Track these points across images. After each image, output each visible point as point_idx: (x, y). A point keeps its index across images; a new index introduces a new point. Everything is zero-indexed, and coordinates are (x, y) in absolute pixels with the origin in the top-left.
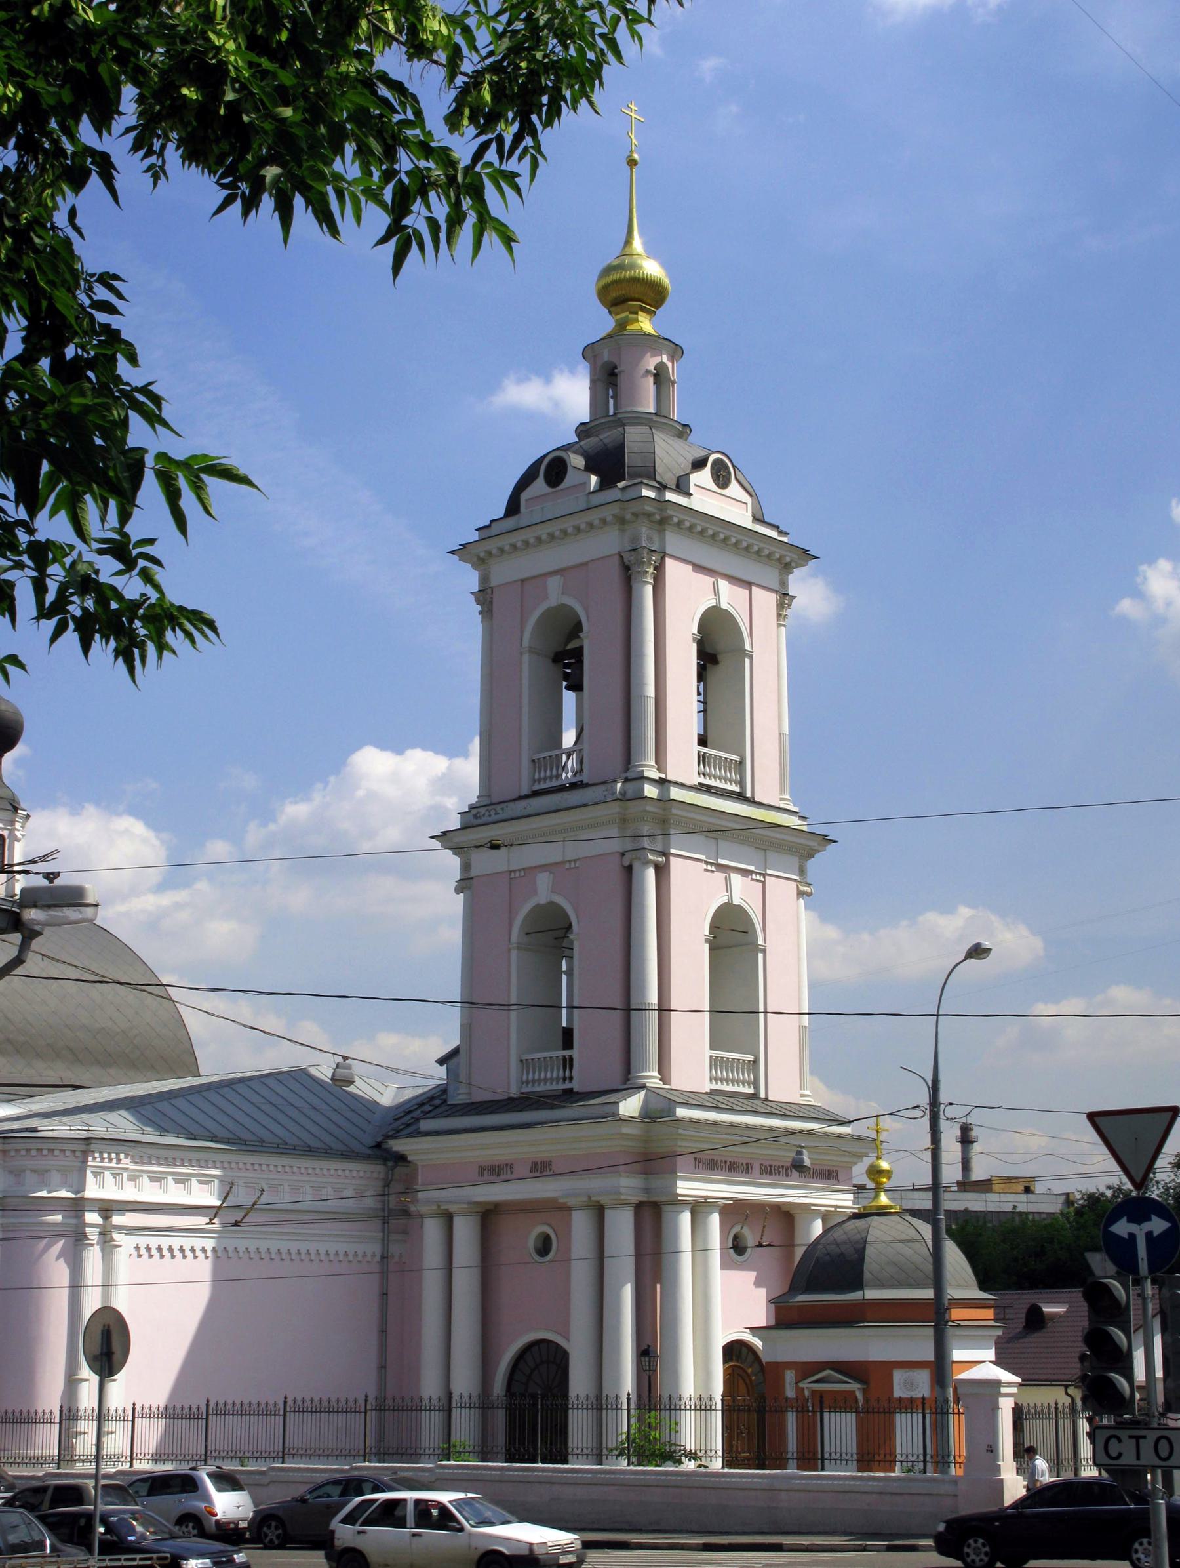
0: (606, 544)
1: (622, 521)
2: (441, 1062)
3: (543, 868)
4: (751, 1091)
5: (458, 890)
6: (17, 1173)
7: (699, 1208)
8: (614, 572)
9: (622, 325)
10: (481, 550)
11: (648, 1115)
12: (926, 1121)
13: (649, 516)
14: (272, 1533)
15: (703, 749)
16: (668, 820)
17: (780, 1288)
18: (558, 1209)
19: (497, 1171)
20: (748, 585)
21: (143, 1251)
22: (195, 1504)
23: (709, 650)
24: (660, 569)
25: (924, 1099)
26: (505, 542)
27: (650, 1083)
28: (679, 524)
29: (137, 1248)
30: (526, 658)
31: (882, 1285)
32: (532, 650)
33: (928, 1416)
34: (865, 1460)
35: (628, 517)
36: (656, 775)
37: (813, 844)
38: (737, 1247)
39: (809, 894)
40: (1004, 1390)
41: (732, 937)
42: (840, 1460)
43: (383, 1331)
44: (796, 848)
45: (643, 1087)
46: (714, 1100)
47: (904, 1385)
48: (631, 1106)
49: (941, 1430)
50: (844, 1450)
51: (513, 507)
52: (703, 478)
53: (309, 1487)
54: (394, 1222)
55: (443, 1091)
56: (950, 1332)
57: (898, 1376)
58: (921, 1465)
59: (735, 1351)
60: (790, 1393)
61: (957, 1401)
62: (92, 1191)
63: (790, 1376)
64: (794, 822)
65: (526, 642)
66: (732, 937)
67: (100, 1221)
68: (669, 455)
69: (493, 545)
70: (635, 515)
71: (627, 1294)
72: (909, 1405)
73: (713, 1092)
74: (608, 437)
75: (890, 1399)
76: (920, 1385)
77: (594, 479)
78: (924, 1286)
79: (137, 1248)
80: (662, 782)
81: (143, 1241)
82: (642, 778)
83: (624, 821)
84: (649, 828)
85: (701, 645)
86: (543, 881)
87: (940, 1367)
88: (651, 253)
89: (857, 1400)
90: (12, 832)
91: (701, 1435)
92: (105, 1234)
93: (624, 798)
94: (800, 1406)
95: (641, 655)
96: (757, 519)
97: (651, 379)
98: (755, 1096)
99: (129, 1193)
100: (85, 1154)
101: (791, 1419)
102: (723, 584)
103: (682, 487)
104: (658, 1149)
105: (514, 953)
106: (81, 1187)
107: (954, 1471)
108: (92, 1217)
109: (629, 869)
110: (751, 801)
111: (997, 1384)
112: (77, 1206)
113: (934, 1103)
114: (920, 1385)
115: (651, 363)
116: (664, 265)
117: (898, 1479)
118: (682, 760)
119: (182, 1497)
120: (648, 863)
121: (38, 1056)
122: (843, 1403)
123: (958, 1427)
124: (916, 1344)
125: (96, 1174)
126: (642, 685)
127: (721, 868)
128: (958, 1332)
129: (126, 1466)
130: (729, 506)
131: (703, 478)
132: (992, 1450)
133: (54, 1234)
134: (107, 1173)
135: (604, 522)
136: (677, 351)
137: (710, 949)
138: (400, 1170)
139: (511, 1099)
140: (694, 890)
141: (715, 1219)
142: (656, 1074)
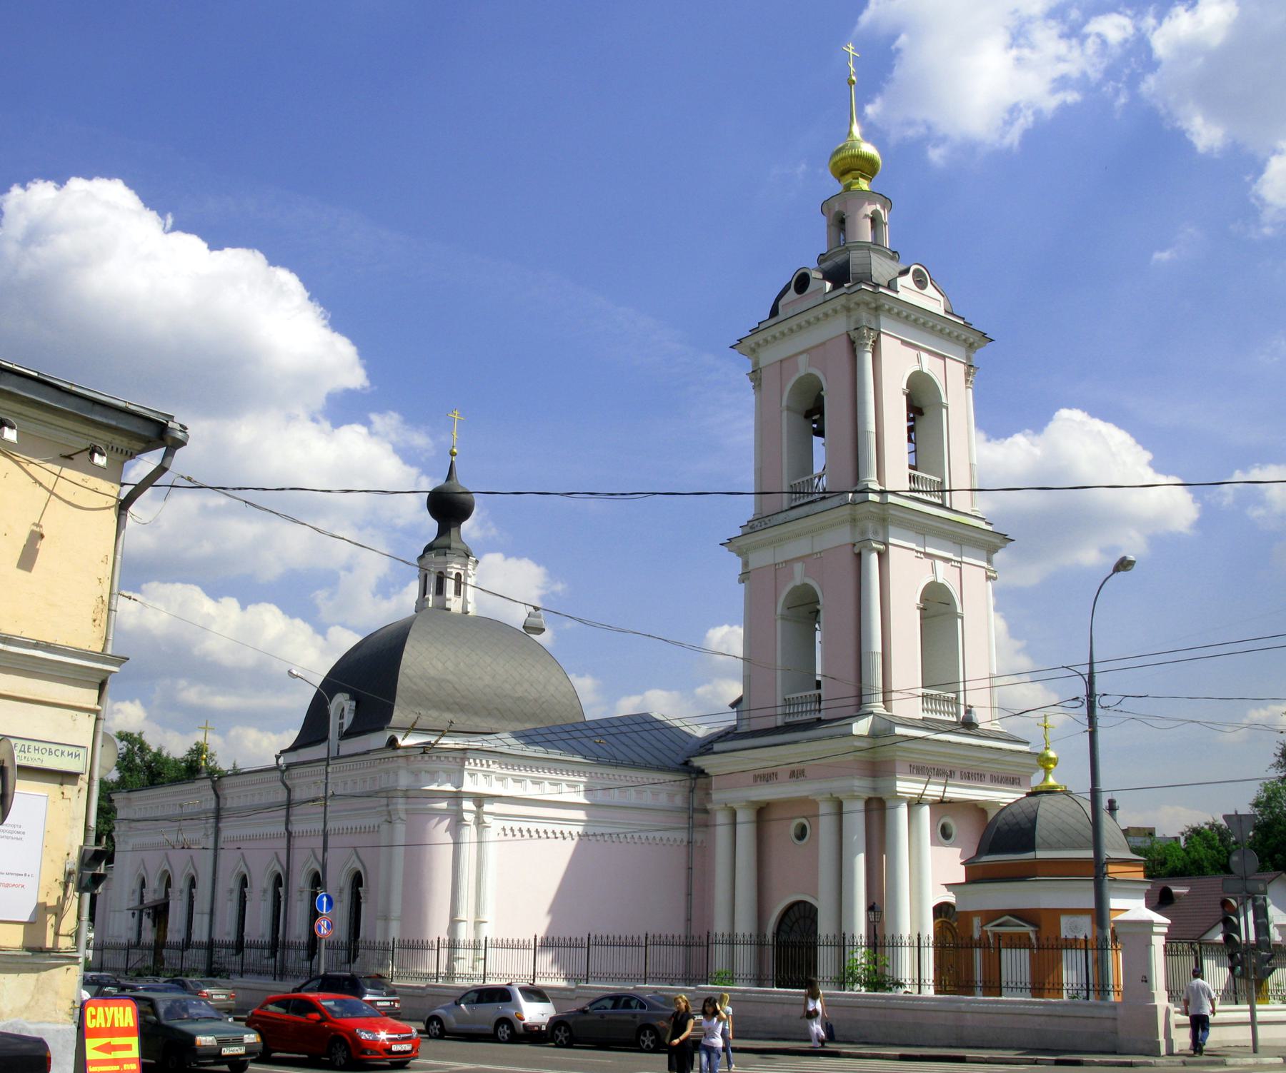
0: (838, 327)
1: (848, 309)
2: (733, 705)
5: (742, 581)
6: (416, 774)
7: (915, 803)
8: (844, 345)
9: (848, 188)
10: (751, 342)
11: (874, 734)
12: (1084, 710)
13: (867, 304)
14: (562, 1035)
15: (913, 472)
16: (887, 517)
17: (972, 853)
18: (807, 805)
19: (767, 777)
20: (944, 357)
21: (508, 831)
22: (511, 1012)
23: (916, 404)
24: (876, 343)
25: (1082, 691)
26: (767, 334)
27: (876, 711)
28: (890, 310)
29: (504, 829)
30: (785, 414)
31: (1050, 847)
32: (788, 408)
33: (1090, 952)
34: (1038, 988)
35: (852, 306)
36: (878, 488)
37: (997, 541)
38: (945, 834)
39: (995, 579)
40: (1156, 929)
41: (938, 608)
42: (1015, 988)
43: (689, 894)
44: (987, 542)
45: (871, 713)
46: (925, 724)
47: (1067, 927)
48: (861, 727)
49: (1101, 964)
51: (774, 312)
52: (907, 281)
53: (588, 1001)
54: (697, 816)
55: (735, 727)
56: (1107, 884)
57: (1065, 921)
58: (1085, 993)
59: (941, 910)
60: (976, 935)
61: (1115, 939)
62: (468, 786)
63: (976, 922)
64: (983, 525)
65: (784, 403)
66: (938, 608)
67: (474, 808)
68: (881, 268)
69: (759, 338)
70: (858, 304)
71: (860, 860)
72: (1072, 944)
73: (924, 719)
74: (839, 259)
75: (1058, 938)
76: (1083, 928)
77: (828, 285)
78: (1087, 848)
79: (504, 829)
80: (882, 492)
81: (508, 825)
82: (866, 490)
83: (854, 521)
84: (871, 520)
85: (910, 398)
86: (798, 568)
87: (1099, 913)
88: (867, 137)
89: (1029, 938)
90: (466, 571)
91: (916, 971)
92: (479, 822)
93: (854, 503)
94: (983, 944)
95: (864, 402)
96: (946, 312)
99: (496, 789)
100: (463, 760)
101: (978, 953)
102: (924, 356)
103: (891, 285)
104: (881, 756)
105: (779, 622)
106: (460, 784)
107: (1113, 997)
108: (468, 805)
109: (859, 555)
110: (950, 509)
111: (1150, 924)
112: (457, 797)
113: (1091, 695)
114: (1083, 928)
115: (869, 209)
116: (879, 150)
117: (1066, 1004)
118: (897, 473)
119: (500, 1006)
120: (873, 549)
121: (476, 714)
122: (1018, 942)
123: (1116, 963)
124: (1080, 895)
125: (471, 775)
126: (865, 423)
127: (928, 555)
128: (1115, 885)
129: (480, 982)
130: (931, 301)
131: (907, 281)
132: (1146, 980)
133: (442, 814)
134: (480, 775)
135: (835, 311)
136: (887, 202)
137: (922, 618)
138: (701, 781)
139: (777, 728)
140: (907, 571)
141: (926, 811)
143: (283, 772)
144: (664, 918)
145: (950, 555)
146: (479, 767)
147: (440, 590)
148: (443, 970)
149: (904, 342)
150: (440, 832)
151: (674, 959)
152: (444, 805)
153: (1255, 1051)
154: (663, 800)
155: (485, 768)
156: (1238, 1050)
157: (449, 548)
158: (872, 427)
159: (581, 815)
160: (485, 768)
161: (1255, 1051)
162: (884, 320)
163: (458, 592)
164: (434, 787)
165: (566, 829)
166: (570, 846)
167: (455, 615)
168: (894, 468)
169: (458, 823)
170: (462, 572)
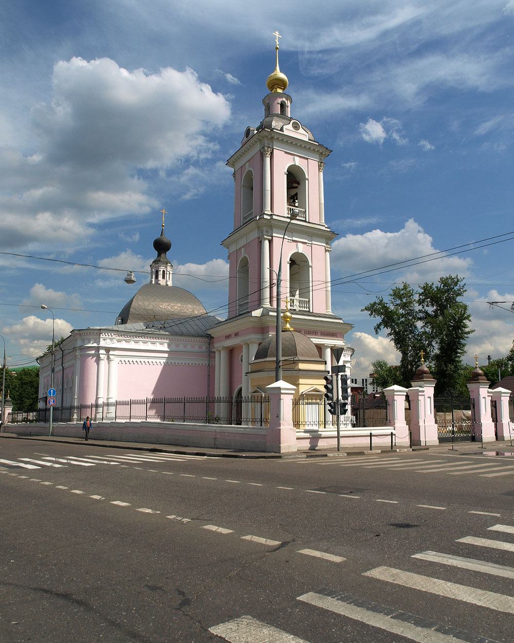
3: (242, 247)
4: (308, 310)
11: (263, 315)
13: (267, 137)
16: (273, 225)
20: (307, 159)
24: (272, 153)
28: (278, 139)
42: (247, 422)
45: (263, 307)
50: (307, 421)
52: (290, 127)
92: (108, 358)
97: (279, 105)
98: (309, 311)
100: (100, 334)
106: (98, 342)
110: (309, 222)
112: (98, 349)
115: (279, 101)
133: (93, 355)
142: (269, 303)
143: (60, 344)
144: (196, 391)
145: (306, 241)
146: (107, 336)
147: (157, 277)
148: (93, 416)
149: (286, 152)
150: (91, 362)
151: (200, 409)
152: (93, 352)
153: (338, 450)
154: (196, 349)
155: (110, 337)
156: (331, 450)
157: (160, 261)
158: (268, 188)
159: (166, 355)
160: (110, 337)
161: (338, 450)
162: (275, 143)
163: (163, 277)
164: (90, 345)
165: (158, 361)
166: (160, 368)
167: (163, 286)
168: (280, 207)
169: (98, 360)
170: (165, 270)
